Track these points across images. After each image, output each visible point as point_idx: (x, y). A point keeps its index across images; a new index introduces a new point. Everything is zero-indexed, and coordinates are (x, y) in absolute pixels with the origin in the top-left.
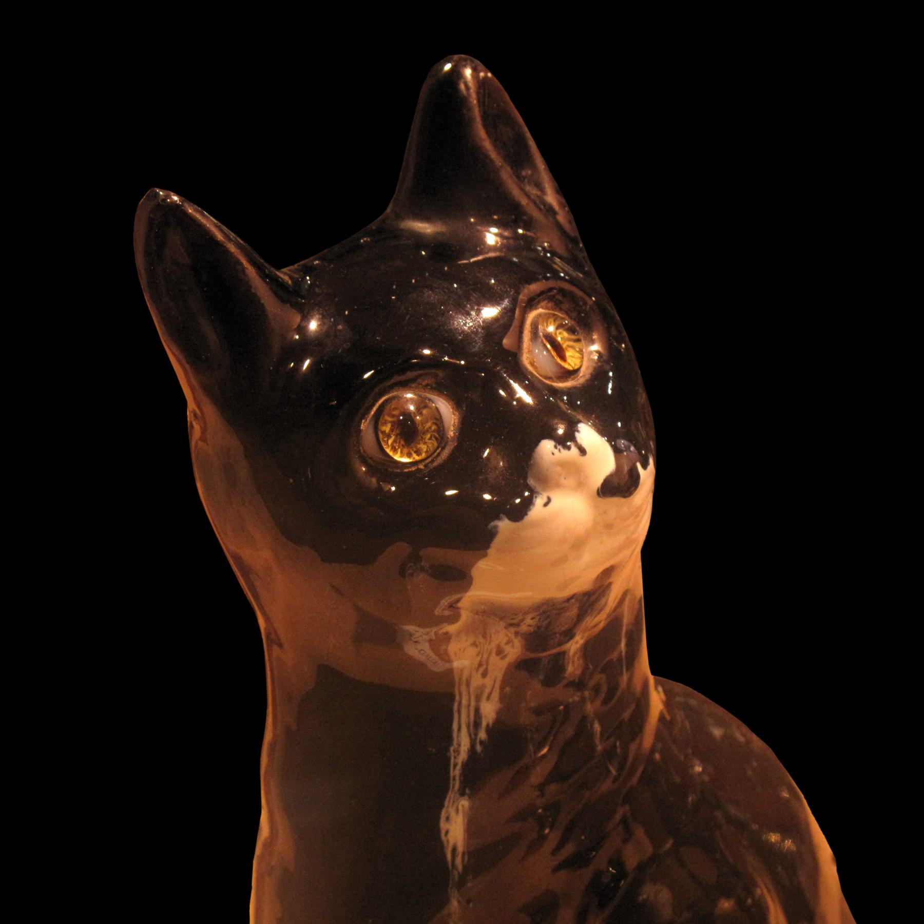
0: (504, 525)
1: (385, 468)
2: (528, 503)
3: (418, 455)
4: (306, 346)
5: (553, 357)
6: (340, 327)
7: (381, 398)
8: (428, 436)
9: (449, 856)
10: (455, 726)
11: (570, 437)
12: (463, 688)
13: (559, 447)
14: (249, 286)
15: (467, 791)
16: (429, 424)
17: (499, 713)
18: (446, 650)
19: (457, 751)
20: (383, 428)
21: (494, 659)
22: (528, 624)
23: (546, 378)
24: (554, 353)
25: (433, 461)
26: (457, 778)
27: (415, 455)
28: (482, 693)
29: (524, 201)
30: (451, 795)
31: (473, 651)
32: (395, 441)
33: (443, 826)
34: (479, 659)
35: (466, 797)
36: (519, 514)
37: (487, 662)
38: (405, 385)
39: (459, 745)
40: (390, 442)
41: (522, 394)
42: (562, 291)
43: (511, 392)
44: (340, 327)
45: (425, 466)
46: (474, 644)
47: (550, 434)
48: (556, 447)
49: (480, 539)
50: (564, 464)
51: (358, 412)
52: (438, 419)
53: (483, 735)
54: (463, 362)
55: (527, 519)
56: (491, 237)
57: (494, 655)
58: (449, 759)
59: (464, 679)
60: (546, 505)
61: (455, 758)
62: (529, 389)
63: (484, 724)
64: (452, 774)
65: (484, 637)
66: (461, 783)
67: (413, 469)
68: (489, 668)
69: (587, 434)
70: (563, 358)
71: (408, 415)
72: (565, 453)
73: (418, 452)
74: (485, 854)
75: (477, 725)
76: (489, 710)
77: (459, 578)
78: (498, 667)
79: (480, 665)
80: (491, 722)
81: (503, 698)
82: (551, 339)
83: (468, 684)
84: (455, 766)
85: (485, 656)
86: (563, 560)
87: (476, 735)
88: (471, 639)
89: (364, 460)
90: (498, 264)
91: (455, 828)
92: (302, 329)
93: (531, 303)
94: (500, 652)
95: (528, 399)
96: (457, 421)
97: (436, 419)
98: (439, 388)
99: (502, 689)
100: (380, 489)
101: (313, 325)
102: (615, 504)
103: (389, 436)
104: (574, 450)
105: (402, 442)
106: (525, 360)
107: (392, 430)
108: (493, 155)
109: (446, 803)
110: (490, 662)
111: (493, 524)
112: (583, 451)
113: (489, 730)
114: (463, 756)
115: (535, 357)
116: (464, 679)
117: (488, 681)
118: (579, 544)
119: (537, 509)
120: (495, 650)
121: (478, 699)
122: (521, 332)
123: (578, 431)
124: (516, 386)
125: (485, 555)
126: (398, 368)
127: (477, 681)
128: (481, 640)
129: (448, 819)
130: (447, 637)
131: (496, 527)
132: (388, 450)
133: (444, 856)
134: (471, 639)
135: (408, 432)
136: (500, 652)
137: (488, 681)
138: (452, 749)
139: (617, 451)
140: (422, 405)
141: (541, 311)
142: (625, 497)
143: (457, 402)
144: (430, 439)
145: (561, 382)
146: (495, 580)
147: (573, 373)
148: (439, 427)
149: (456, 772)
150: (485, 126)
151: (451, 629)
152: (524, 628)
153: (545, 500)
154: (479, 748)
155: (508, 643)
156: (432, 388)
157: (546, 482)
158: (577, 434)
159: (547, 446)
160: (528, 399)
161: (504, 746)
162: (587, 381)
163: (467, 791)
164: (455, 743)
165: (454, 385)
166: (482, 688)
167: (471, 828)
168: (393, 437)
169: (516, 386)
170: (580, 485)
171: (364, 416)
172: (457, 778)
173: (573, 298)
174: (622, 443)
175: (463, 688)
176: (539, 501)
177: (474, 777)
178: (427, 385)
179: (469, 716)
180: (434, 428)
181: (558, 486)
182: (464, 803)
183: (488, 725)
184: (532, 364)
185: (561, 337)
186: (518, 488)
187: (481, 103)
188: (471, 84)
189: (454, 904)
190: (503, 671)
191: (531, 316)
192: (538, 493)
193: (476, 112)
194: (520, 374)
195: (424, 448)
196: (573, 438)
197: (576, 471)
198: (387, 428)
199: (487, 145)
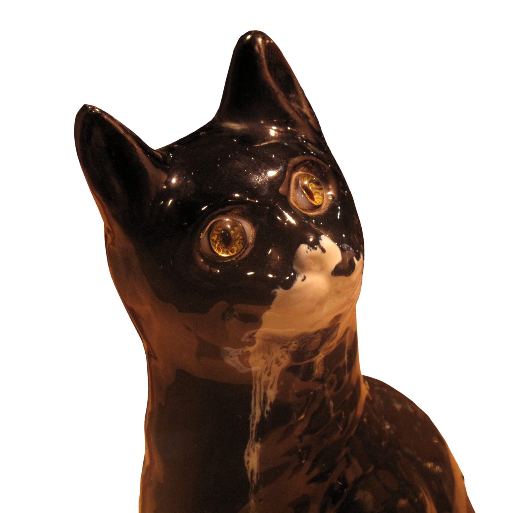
0: (280, 291)
1: (214, 260)
2: (293, 279)
3: (232, 253)
4: (170, 192)
6: (189, 182)
7: (211, 221)
8: (238, 242)
10: (253, 403)
11: (316, 243)
12: (257, 382)
13: (310, 248)
14: (138, 159)
15: (260, 439)
16: (238, 236)
17: (277, 396)
18: (248, 361)
19: (254, 417)
20: (213, 238)
21: (274, 366)
22: (293, 346)
23: (303, 210)
24: (307, 196)
25: (240, 256)
26: (254, 432)
27: (230, 253)
28: (268, 385)
29: (291, 112)
30: (250, 441)
31: (262, 361)
32: (219, 245)
33: (246, 458)
34: (266, 366)
35: (259, 443)
36: (288, 285)
37: (270, 367)
38: (225, 214)
39: (255, 414)
40: (217, 245)
41: (289, 218)
42: (312, 162)
43: (284, 218)
44: (189, 182)
46: (263, 358)
47: (305, 241)
48: (308, 248)
49: (266, 299)
51: (198, 228)
52: (243, 232)
53: (268, 408)
54: (257, 201)
55: (293, 288)
56: (273, 132)
57: (274, 363)
58: (249, 421)
60: (303, 280)
61: (253, 421)
62: (294, 216)
63: (269, 402)
65: (269, 354)
66: (256, 435)
68: (272, 371)
69: (326, 241)
70: (313, 199)
71: (227, 231)
72: (314, 252)
73: (232, 251)
74: (269, 474)
75: (265, 402)
76: (272, 394)
77: (255, 321)
78: (277, 370)
79: (267, 369)
80: (272, 401)
81: (279, 388)
82: (306, 188)
83: (260, 380)
84: (253, 425)
85: (269, 365)
86: (313, 311)
87: (264, 408)
88: (261, 355)
89: (202, 256)
90: (276, 147)
91: (253, 460)
92: (168, 183)
93: (295, 168)
94: (277, 362)
95: (293, 222)
96: (253, 234)
97: (242, 232)
98: (244, 216)
99: (279, 382)
100: (211, 271)
101: (174, 181)
102: (341, 280)
103: (216, 242)
104: (319, 250)
105: (223, 246)
106: (292, 200)
107: (217, 239)
108: (274, 86)
109: (248, 446)
111: (273, 291)
112: (323, 251)
113: (271, 405)
114: (257, 420)
115: (297, 198)
117: (271, 378)
118: (321, 302)
119: (298, 282)
120: (275, 361)
121: (265, 388)
122: (289, 185)
123: (321, 239)
124: (286, 214)
125: (269, 308)
126: (221, 204)
127: (265, 378)
128: (267, 355)
129: (248, 455)
130: (248, 354)
131: (275, 292)
132: (215, 250)
133: (247, 475)
134: (261, 355)
135: (227, 240)
136: (277, 362)
137: (271, 378)
138: (251, 416)
139: (342, 250)
140: (234, 225)
141: (300, 172)
142: (347, 276)
143: (254, 223)
146: (275, 322)
147: (319, 206)
149: (253, 429)
150: (269, 70)
151: (251, 349)
152: (291, 349)
153: (303, 277)
154: (266, 415)
155: (282, 357)
156: (240, 215)
157: (303, 267)
158: (320, 241)
159: (304, 248)
160: (293, 222)
161: (280, 414)
162: (326, 211)
163: (260, 439)
164: (253, 412)
165: (252, 214)
166: (268, 382)
167: (262, 460)
168: (218, 243)
169: (286, 214)
170: (322, 269)
171: (202, 231)
172: (254, 432)
173: (318, 165)
174: (345, 246)
175: (257, 382)
176: (299, 278)
177: (263, 432)
180: (241, 237)
181: (310, 270)
182: (258, 446)
183: (271, 403)
184: (295, 202)
185: (312, 187)
186: (288, 270)
187: (267, 57)
188: (261, 47)
189: (252, 502)
191: (295, 175)
192: (299, 274)
193: (265, 62)
194: (289, 208)
195: (235, 248)
196: (318, 243)
197: (320, 262)
198: (215, 238)
199: (271, 80)
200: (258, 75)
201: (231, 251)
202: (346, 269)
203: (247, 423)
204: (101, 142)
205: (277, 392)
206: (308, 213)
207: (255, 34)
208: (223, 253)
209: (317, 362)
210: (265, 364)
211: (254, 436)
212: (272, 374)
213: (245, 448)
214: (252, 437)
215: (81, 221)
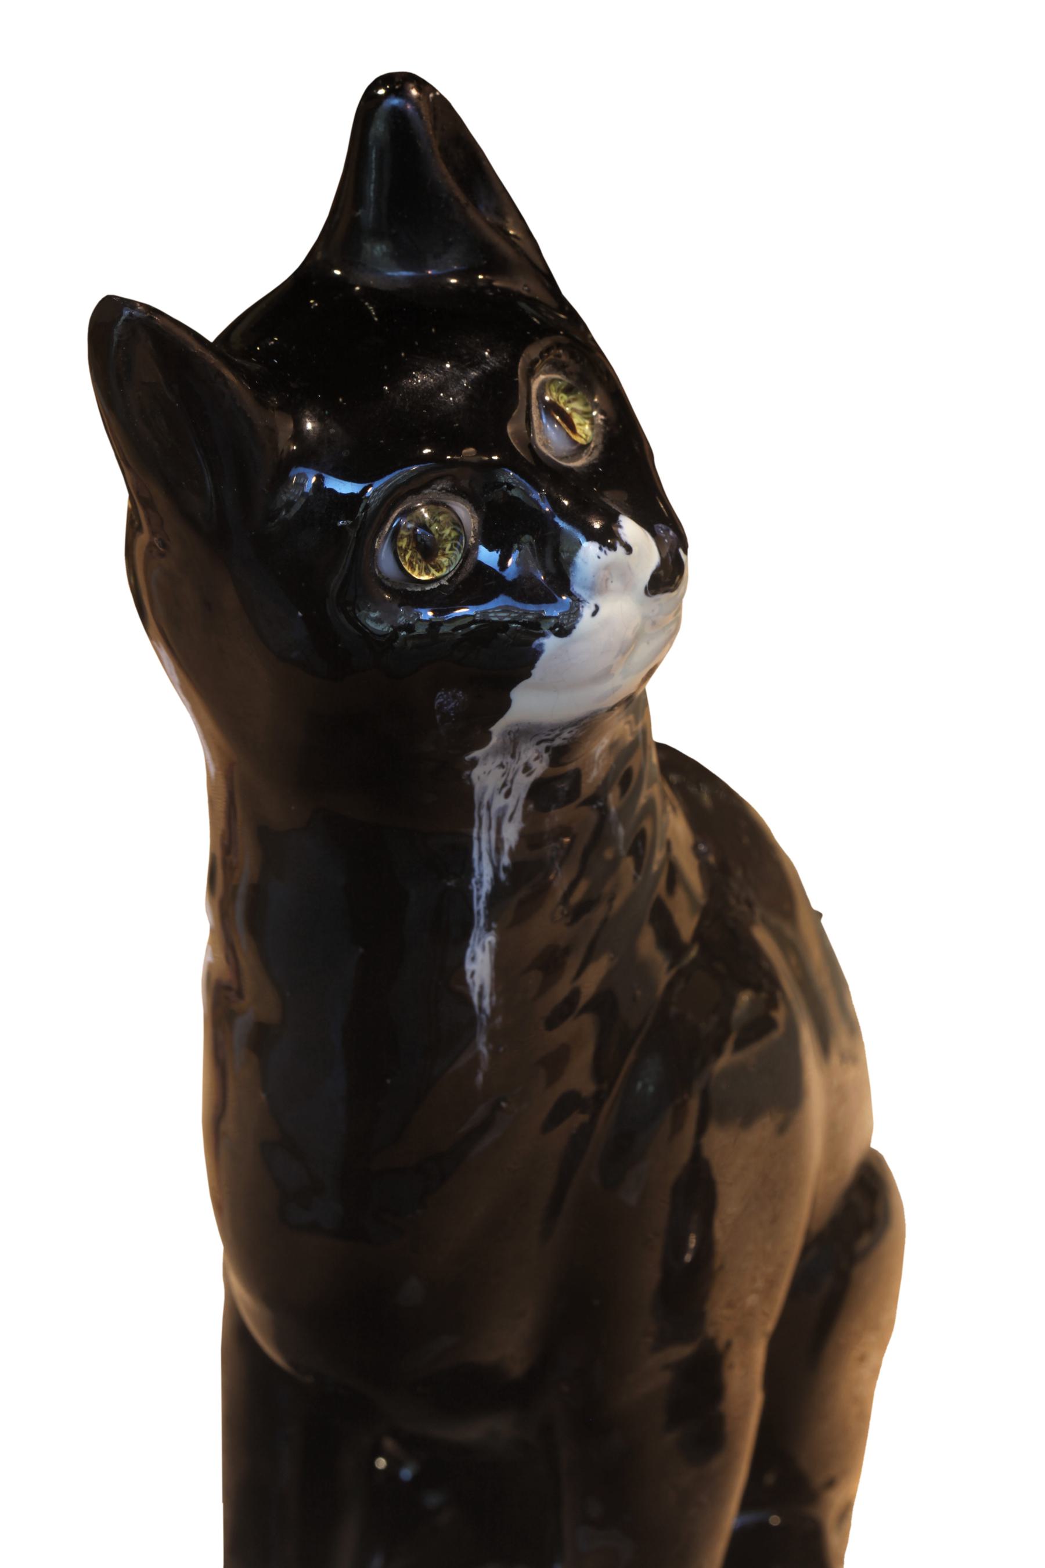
0: (550, 643)
2: (574, 613)
3: (438, 571)
5: (568, 434)
6: (332, 431)
7: (394, 511)
8: (448, 546)
9: (475, 999)
10: (475, 855)
12: (484, 812)
13: (604, 549)
15: (494, 925)
16: (447, 531)
17: (523, 835)
18: (469, 776)
19: (480, 883)
20: (400, 544)
23: (562, 458)
24: (564, 426)
27: (433, 571)
28: (504, 815)
30: (476, 933)
32: (412, 557)
33: (469, 966)
35: (493, 932)
36: (563, 630)
37: (512, 781)
39: (481, 875)
40: (407, 557)
44: (332, 431)
45: (448, 581)
46: (502, 766)
48: (600, 549)
50: (607, 568)
52: (457, 524)
53: (506, 860)
55: (575, 632)
57: (520, 772)
58: (471, 892)
59: (485, 802)
60: (594, 614)
61: (478, 890)
63: (506, 847)
64: (475, 908)
65: (513, 756)
66: (487, 917)
67: (435, 585)
68: (514, 788)
72: (611, 554)
73: (438, 568)
75: (499, 849)
76: (511, 833)
78: (523, 783)
79: (504, 785)
80: (513, 846)
81: (526, 817)
83: (489, 808)
84: (479, 898)
85: (510, 778)
87: (499, 861)
91: (479, 964)
94: (527, 769)
96: (476, 525)
97: (454, 524)
99: (525, 806)
103: (406, 551)
104: (620, 549)
105: (419, 557)
107: (408, 545)
109: (471, 942)
110: (515, 780)
111: (537, 642)
112: (629, 549)
113: (512, 854)
114: (486, 887)
116: (485, 802)
117: (511, 801)
119: (586, 622)
120: (521, 768)
122: (529, 408)
123: (620, 527)
127: (499, 802)
128: (509, 759)
129: (473, 959)
131: (541, 645)
132: (406, 567)
135: (427, 551)
136: (527, 769)
138: (473, 881)
141: (542, 377)
142: (672, 591)
144: (451, 549)
145: (578, 459)
147: (582, 448)
148: (460, 533)
149: (479, 906)
151: (477, 754)
153: (593, 609)
154: (503, 876)
155: (537, 759)
156: (447, 491)
158: (620, 531)
164: (477, 873)
166: (503, 810)
175: (484, 812)
176: (587, 611)
178: (442, 489)
179: (489, 842)
180: (454, 534)
184: (544, 445)
190: (527, 790)
192: (584, 601)
195: (444, 560)
196: (616, 536)
197: (625, 575)
198: (403, 543)
200: (411, 157)
201: (434, 567)
202: (669, 576)
203: (467, 897)
204: (129, 347)
205: (522, 825)
206: (572, 465)
207: (396, 83)
208: (420, 574)
209: (597, 755)
210: (503, 775)
211: (482, 921)
212: (513, 793)
213: (467, 945)
214: (478, 922)
215: (92, 491)
